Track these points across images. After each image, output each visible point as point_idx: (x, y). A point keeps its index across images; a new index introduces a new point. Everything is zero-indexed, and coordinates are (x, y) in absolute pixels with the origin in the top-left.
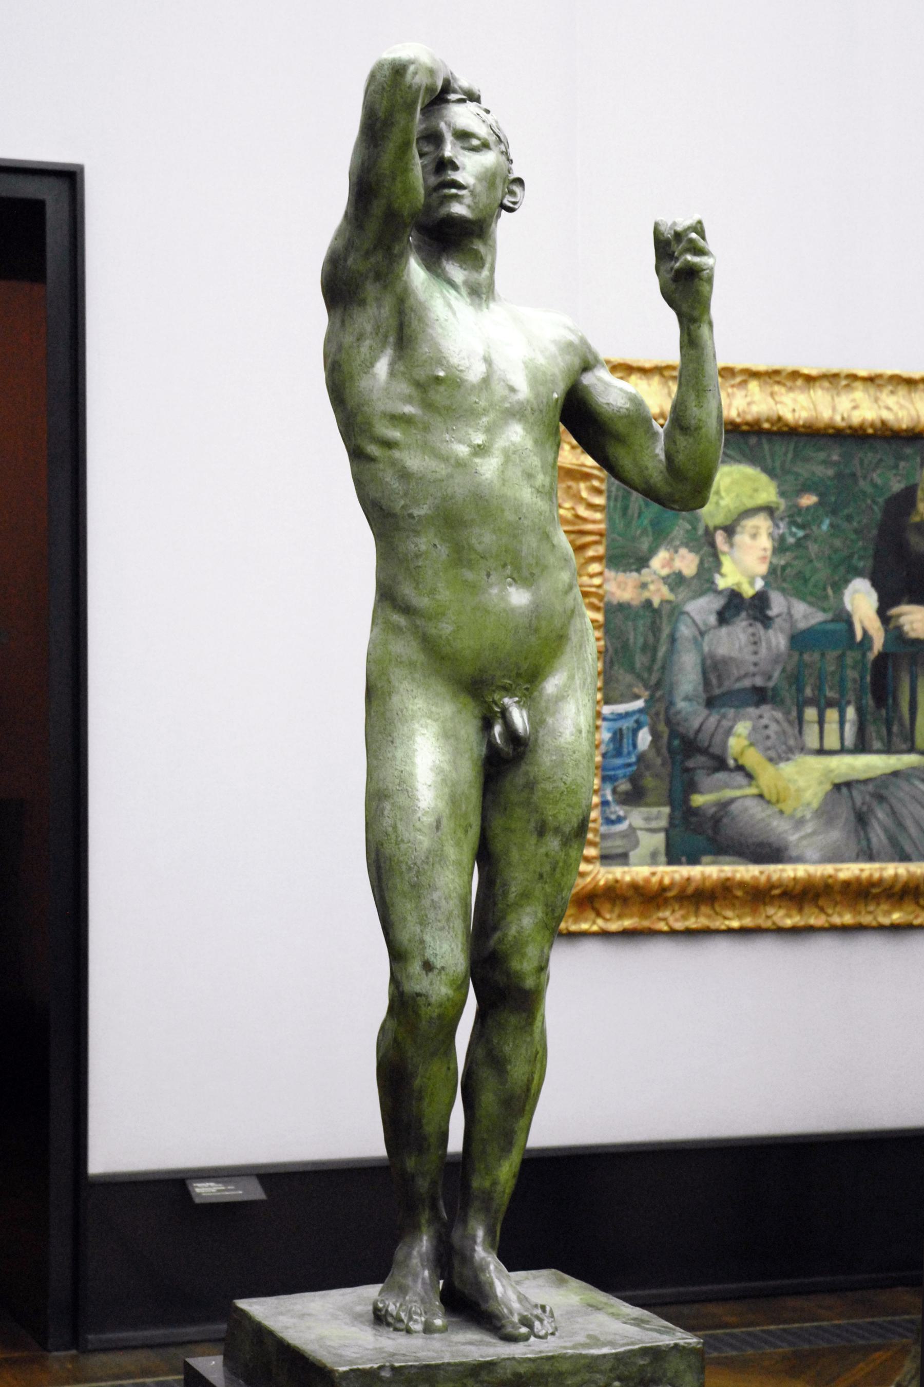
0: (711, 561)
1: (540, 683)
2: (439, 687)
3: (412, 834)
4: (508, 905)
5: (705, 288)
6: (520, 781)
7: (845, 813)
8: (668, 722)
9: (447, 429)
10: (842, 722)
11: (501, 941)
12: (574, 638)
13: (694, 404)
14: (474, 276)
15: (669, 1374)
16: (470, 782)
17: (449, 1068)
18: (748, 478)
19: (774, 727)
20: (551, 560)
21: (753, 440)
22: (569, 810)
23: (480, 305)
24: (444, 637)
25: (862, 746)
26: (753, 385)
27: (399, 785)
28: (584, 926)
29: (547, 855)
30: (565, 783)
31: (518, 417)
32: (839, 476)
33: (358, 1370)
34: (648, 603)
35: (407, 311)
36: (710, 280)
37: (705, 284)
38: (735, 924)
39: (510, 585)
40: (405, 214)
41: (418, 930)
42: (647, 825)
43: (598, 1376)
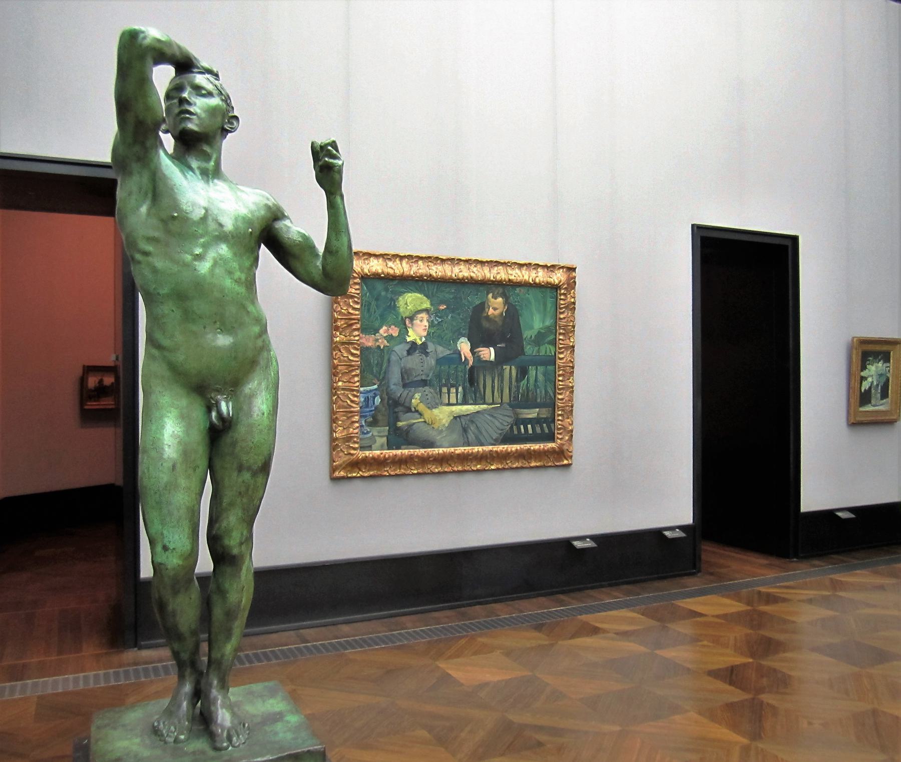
0: (404, 331)
5: (337, 176)
7: (459, 428)
8: (387, 394)
10: (493, 382)
11: (219, 529)
12: (262, 362)
14: (204, 165)
18: (419, 298)
19: (430, 395)
20: (247, 319)
21: (420, 283)
22: (256, 457)
25: (465, 402)
26: (420, 262)
28: (354, 475)
29: (243, 482)
32: (455, 298)
34: (379, 347)
36: (340, 172)
38: (415, 472)
39: (219, 333)
42: (380, 434)
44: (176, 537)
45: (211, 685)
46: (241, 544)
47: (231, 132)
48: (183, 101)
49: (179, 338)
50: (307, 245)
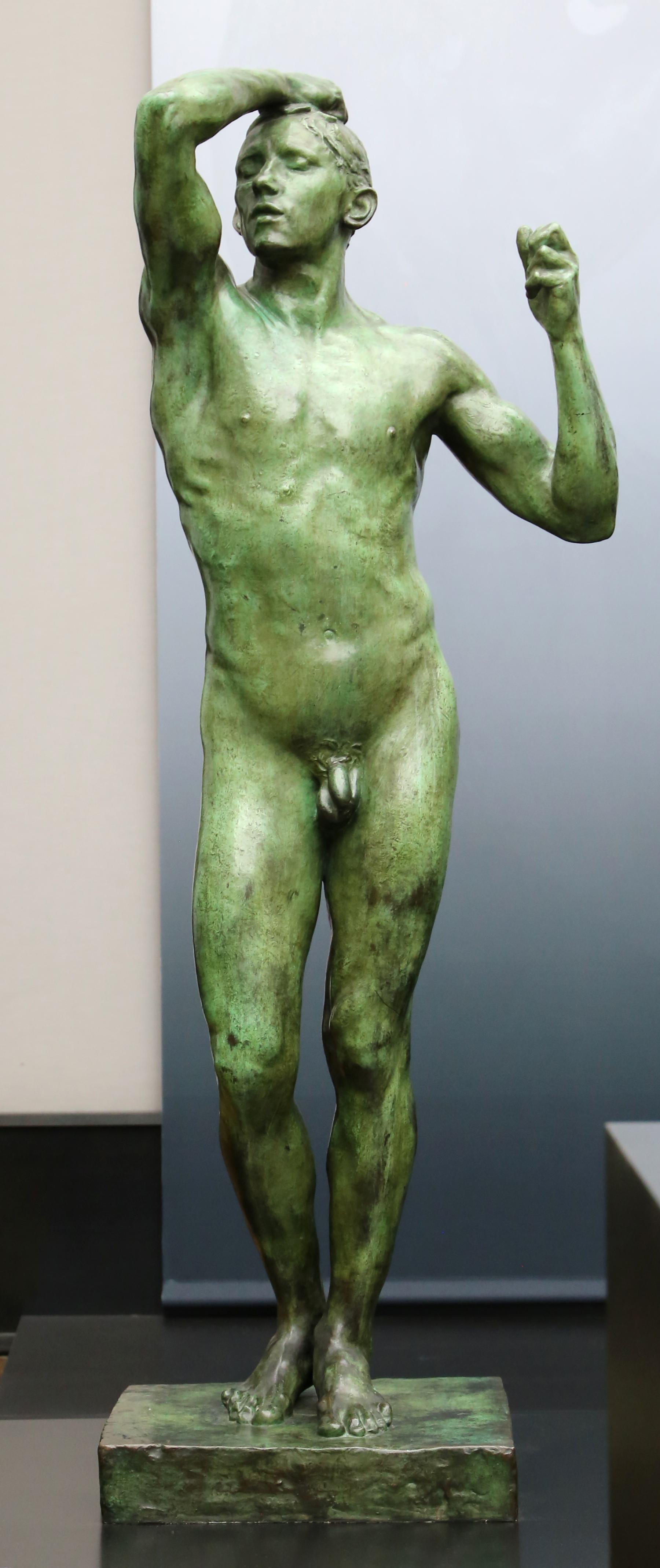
1: (375, 741)
2: (262, 747)
3: (220, 902)
4: (342, 977)
6: (353, 844)
9: (254, 475)
11: (336, 1015)
12: (418, 690)
13: (567, 429)
14: (307, 304)
15: (474, 1480)
16: (296, 846)
17: (288, 1148)
20: (384, 607)
22: (401, 878)
23: (313, 335)
24: (260, 694)
27: (213, 849)
29: (378, 925)
30: (395, 849)
31: (335, 458)
33: (125, 1448)
35: (216, 349)
37: (559, 301)
39: (330, 638)
40: (195, 252)
41: (224, 1002)
43: (390, 1475)
44: (251, 1020)
45: (330, 1332)
46: (377, 1046)
47: (359, 227)
48: (261, 190)
49: (258, 649)
50: (523, 447)
